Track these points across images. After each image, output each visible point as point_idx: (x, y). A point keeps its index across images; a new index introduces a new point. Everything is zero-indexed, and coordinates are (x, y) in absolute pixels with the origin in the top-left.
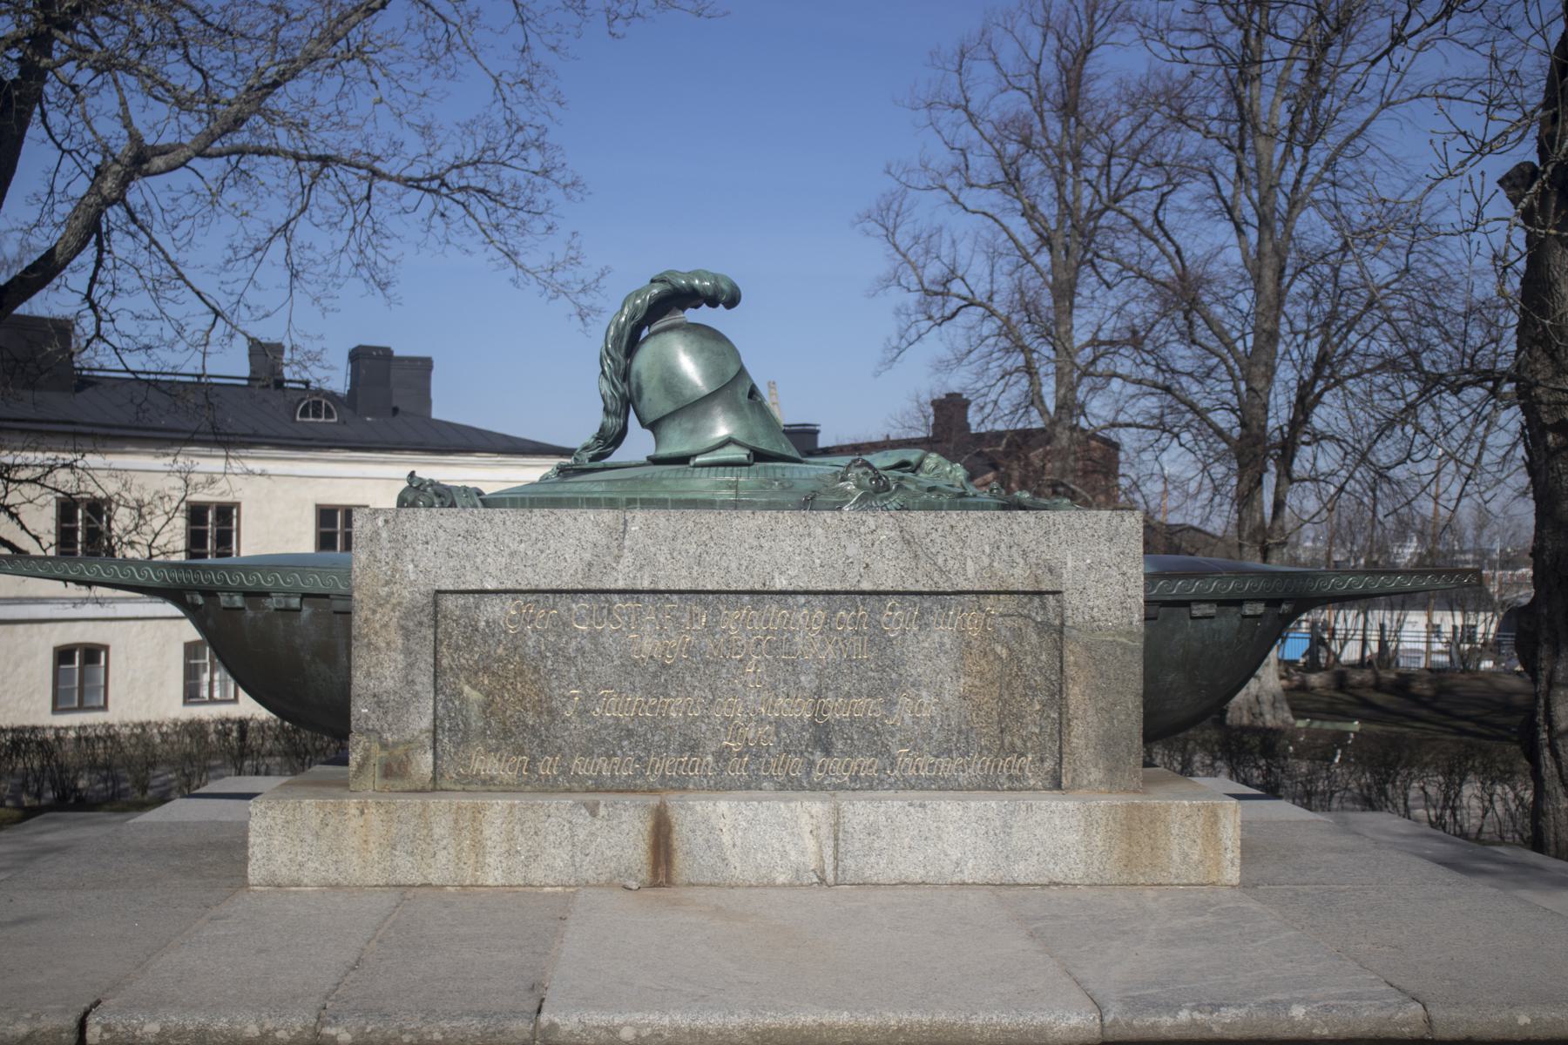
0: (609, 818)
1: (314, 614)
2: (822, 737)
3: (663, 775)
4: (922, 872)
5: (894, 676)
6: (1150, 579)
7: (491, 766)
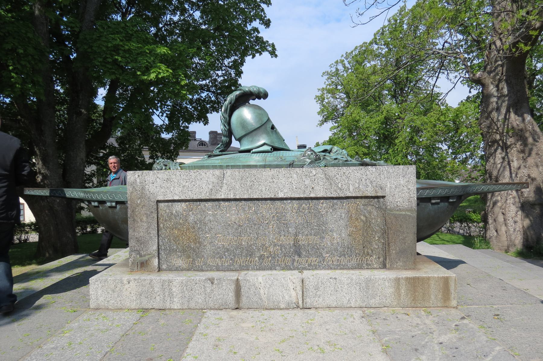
0: (218, 284)
1: (120, 208)
2: (298, 250)
3: (240, 265)
4: (335, 303)
5: (323, 228)
6: (418, 189)
7: (180, 262)
